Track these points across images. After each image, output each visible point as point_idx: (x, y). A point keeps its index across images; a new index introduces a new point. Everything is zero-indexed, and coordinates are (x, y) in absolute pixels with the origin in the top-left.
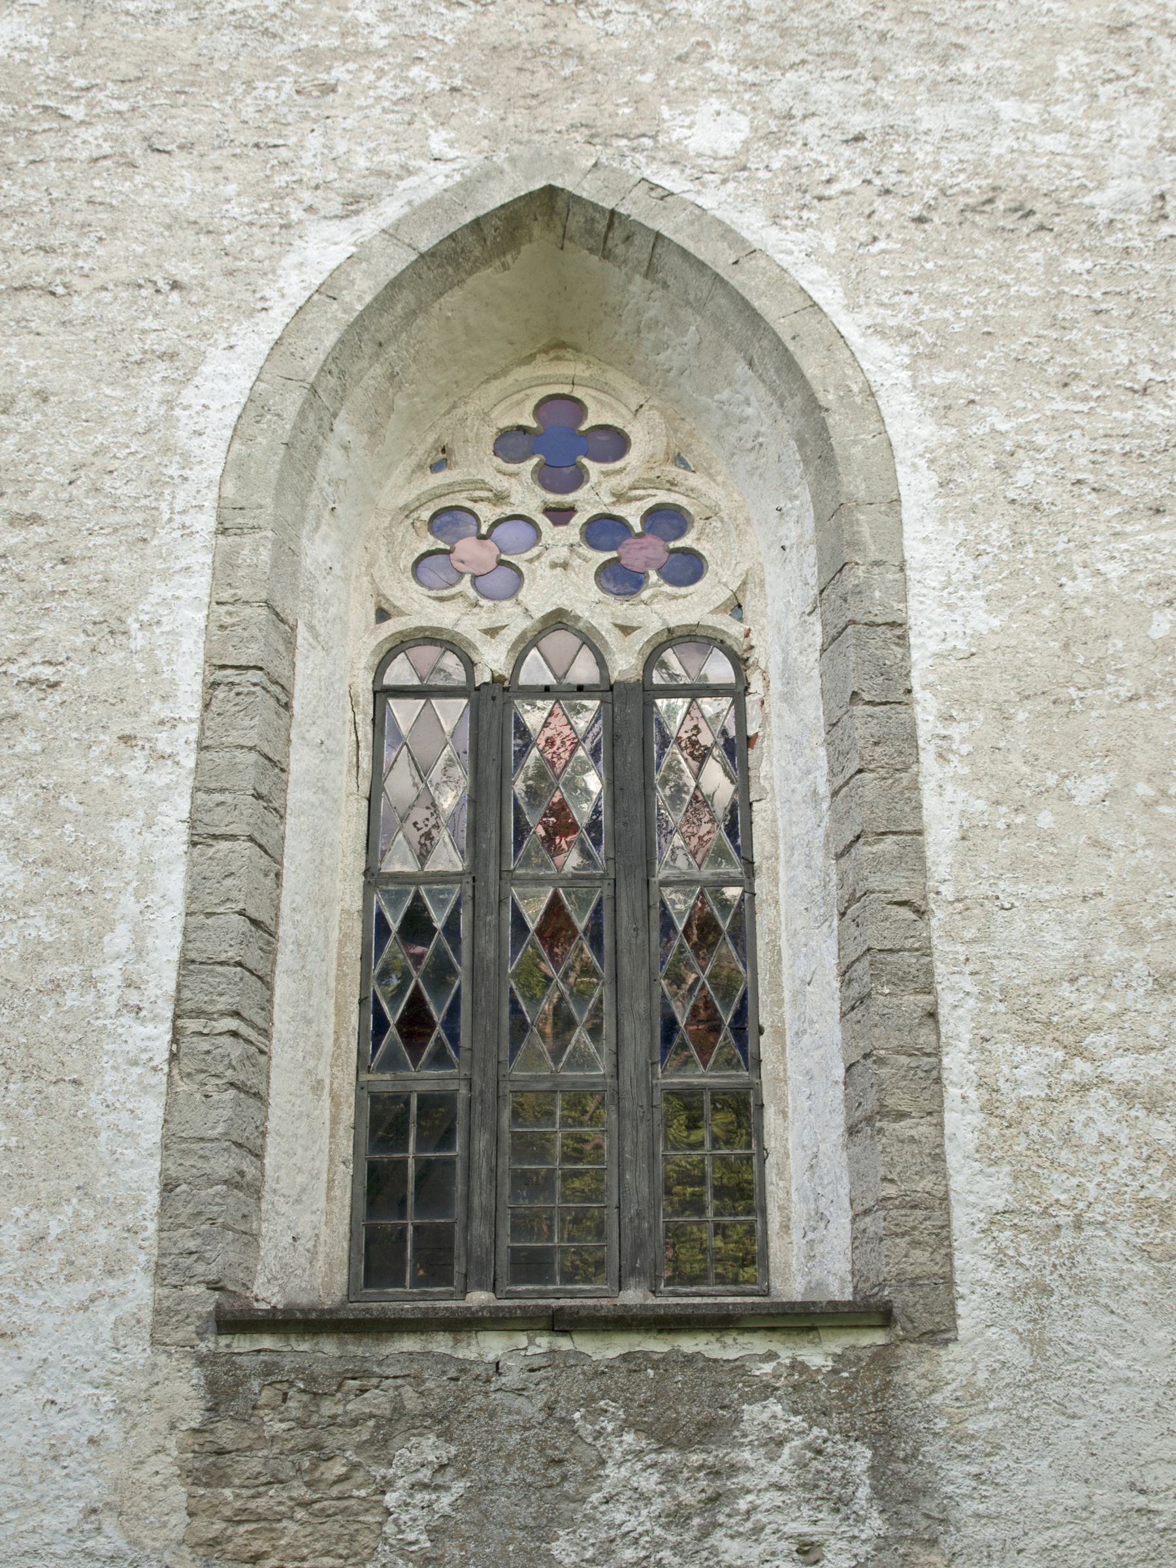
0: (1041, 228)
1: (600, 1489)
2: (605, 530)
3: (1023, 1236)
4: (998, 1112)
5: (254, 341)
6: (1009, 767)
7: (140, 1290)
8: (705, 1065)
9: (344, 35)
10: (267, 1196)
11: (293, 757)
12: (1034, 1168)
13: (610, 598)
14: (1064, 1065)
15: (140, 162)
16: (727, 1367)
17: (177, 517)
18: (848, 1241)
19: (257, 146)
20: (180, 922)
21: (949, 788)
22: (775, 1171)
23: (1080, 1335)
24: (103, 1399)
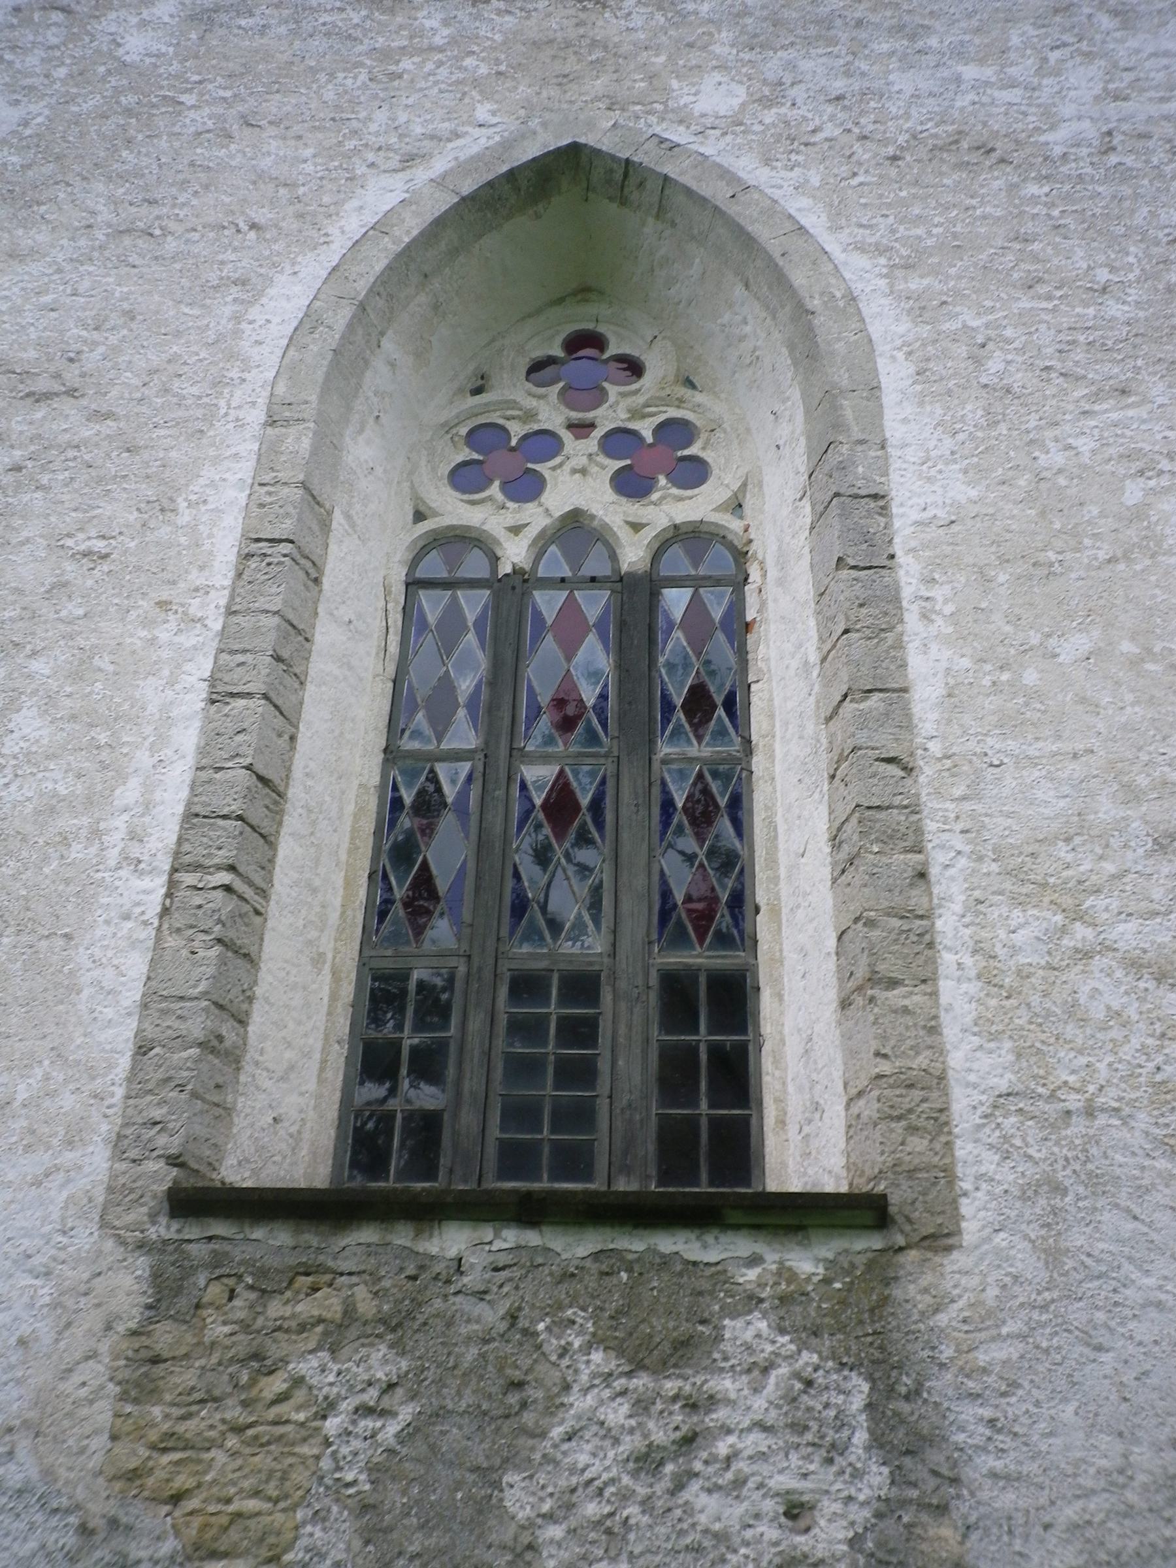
0: (1002, 161)
1: (561, 1423)
2: (619, 440)
3: (1030, 1123)
4: (995, 981)
5: (314, 268)
6: (992, 627)
7: (95, 1163)
8: (701, 945)
9: (411, 37)
10: (248, 1067)
11: (318, 629)
12: (1038, 1045)
13: (624, 500)
14: (1064, 930)
15: (236, 134)
16: (709, 1271)
17: (232, 411)
18: (843, 1130)
19: (333, 119)
20: (188, 777)
21: (934, 647)
22: (770, 1059)
23: (1101, 1245)
24: (41, 1292)
